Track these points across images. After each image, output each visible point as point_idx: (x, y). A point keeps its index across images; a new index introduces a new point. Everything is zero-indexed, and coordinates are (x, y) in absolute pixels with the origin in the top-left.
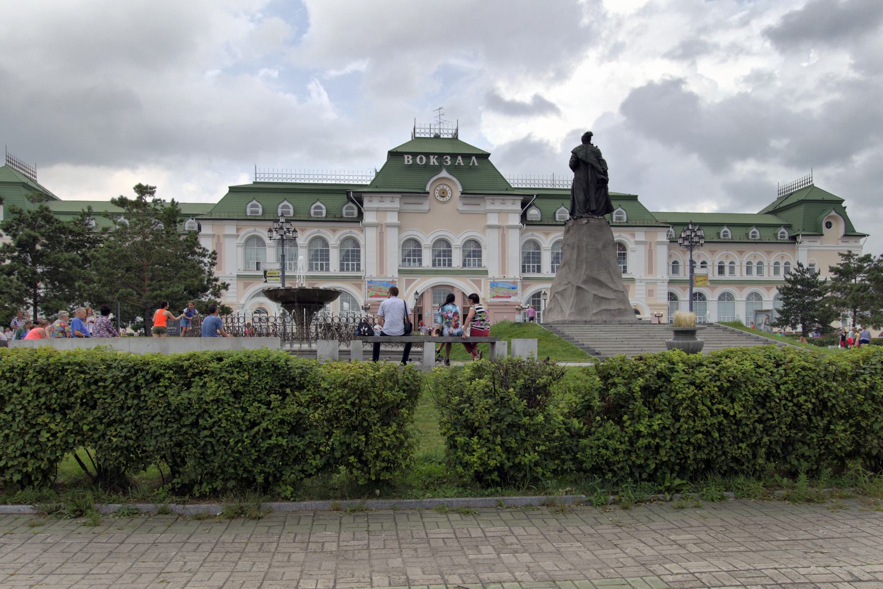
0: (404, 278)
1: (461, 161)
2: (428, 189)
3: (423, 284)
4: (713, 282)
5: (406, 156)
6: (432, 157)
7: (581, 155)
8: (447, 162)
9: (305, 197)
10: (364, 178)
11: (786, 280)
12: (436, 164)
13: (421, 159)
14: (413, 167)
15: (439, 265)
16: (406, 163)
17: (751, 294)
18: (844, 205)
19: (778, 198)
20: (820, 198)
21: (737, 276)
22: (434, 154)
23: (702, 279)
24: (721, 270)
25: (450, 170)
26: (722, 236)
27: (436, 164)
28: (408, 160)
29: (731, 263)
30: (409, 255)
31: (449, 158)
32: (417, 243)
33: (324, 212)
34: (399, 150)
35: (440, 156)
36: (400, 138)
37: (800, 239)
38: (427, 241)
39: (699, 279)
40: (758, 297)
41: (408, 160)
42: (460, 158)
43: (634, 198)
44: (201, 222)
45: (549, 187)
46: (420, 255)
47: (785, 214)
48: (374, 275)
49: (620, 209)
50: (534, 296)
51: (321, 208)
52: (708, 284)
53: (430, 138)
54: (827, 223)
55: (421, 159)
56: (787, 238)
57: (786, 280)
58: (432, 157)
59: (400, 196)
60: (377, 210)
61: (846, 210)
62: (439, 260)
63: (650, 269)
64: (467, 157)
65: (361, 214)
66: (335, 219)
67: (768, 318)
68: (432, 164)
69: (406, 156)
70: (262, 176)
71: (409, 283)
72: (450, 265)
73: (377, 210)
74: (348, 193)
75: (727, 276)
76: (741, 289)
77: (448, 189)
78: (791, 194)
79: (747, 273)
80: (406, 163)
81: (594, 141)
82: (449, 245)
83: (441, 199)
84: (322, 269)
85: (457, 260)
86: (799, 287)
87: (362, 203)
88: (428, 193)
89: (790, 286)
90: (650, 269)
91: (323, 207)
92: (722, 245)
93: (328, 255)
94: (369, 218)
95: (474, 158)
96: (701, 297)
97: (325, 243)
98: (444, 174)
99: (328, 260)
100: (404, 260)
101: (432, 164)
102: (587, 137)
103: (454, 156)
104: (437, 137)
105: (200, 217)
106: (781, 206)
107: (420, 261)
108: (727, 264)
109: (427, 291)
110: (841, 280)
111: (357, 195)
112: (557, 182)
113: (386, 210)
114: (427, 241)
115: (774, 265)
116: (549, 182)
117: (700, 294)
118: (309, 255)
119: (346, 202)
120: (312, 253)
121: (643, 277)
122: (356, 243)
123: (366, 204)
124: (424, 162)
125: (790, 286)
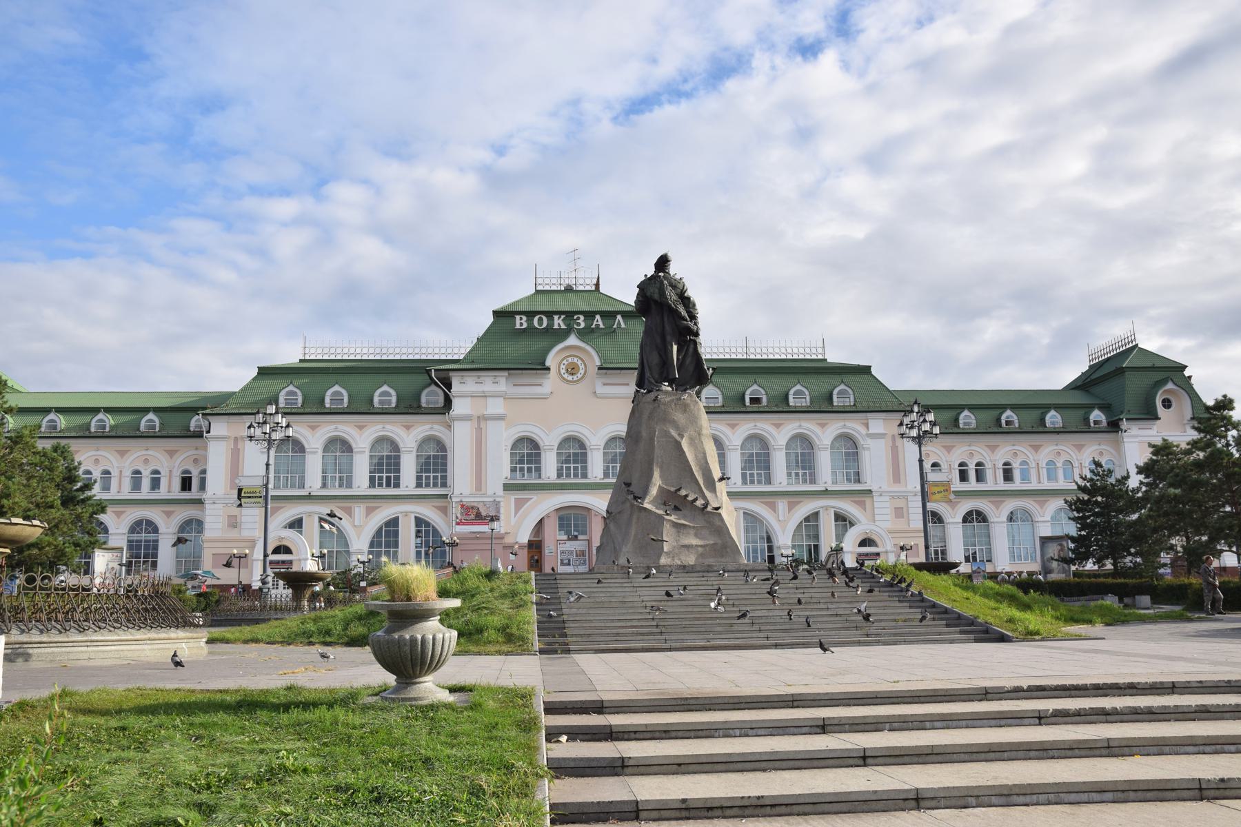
0: (513, 497)
1: (600, 323)
2: (548, 363)
3: (545, 505)
4: (959, 494)
5: (518, 317)
6: (556, 317)
7: (653, 291)
8: (579, 324)
9: (319, 378)
10: (456, 350)
11: (1080, 488)
12: (563, 327)
13: (540, 320)
14: (530, 331)
15: (568, 476)
16: (518, 326)
17: (969, 513)
18: (1187, 373)
19: (1090, 367)
20: (1150, 365)
21: (989, 485)
22: (559, 313)
23: (942, 489)
24: (1008, 475)
25: (582, 334)
26: (748, 403)
27: (563, 327)
28: (521, 322)
29: (978, 464)
30: (521, 462)
31: (582, 318)
32: (533, 444)
33: (394, 400)
34: (511, 309)
35: (569, 315)
36: (515, 292)
37: (1124, 424)
38: (549, 441)
39: (936, 489)
40: (1028, 517)
41: (521, 322)
42: (598, 317)
43: (866, 370)
44: (211, 418)
45: (740, 357)
46: (538, 462)
47: (1097, 390)
48: (466, 492)
49: (842, 387)
50: (807, 519)
51: (390, 395)
52: (952, 497)
53: (560, 291)
54: (1164, 401)
55: (540, 320)
56: (1104, 424)
57: (1080, 488)
58: (556, 317)
59: (506, 373)
60: (473, 396)
61: (1193, 381)
62: (568, 469)
63: (897, 477)
64: (609, 315)
65: (448, 402)
66: (409, 406)
67: (1062, 550)
68: (556, 327)
69: (518, 317)
70: (313, 351)
71: (519, 504)
72: (585, 476)
73: (473, 396)
74: (428, 372)
75: (1017, 484)
76: (997, 505)
77: (579, 362)
78: (1108, 359)
79: (1049, 479)
80: (518, 326)
81: (674, 269)
82: (582, 445)
83: (570, 378)
84: (388, 485)
85: (550, 466)
86: (1099, 499)
87: (449, 386)
88: (548, 369)
89: (1086, 497)
90: (897, 477)
91: (393, 392)
92: (960, 437)
93: (398, 464)
94: (459, 407)
95: (619, 317)
96: (937, 518)
97: (395, 447)
98: (572, 340)
99: (398, 471)
100: (513, 470)
101: (556, 327)
102: (663, 263)
103: (590, 315)
104: (569, 289)
105: (208, 411)
106: (1094, 377)
107: (538, 470)
108: (1016, 465)
109: (548, 516)
110: (1157, 486)
111: (442, 375)
112: (752, 350)
113: (484, 396)
114: (549, 441)
115: (1061, 463)
116: (740, 350)
117: (979, 513)
118: (371, 464)
119: (421, 385)
120: (375, 461)
121: (885, 487)
122: (441, 446)
123: (456, 387)
124: (544, 325)
125: (1086, 497)
